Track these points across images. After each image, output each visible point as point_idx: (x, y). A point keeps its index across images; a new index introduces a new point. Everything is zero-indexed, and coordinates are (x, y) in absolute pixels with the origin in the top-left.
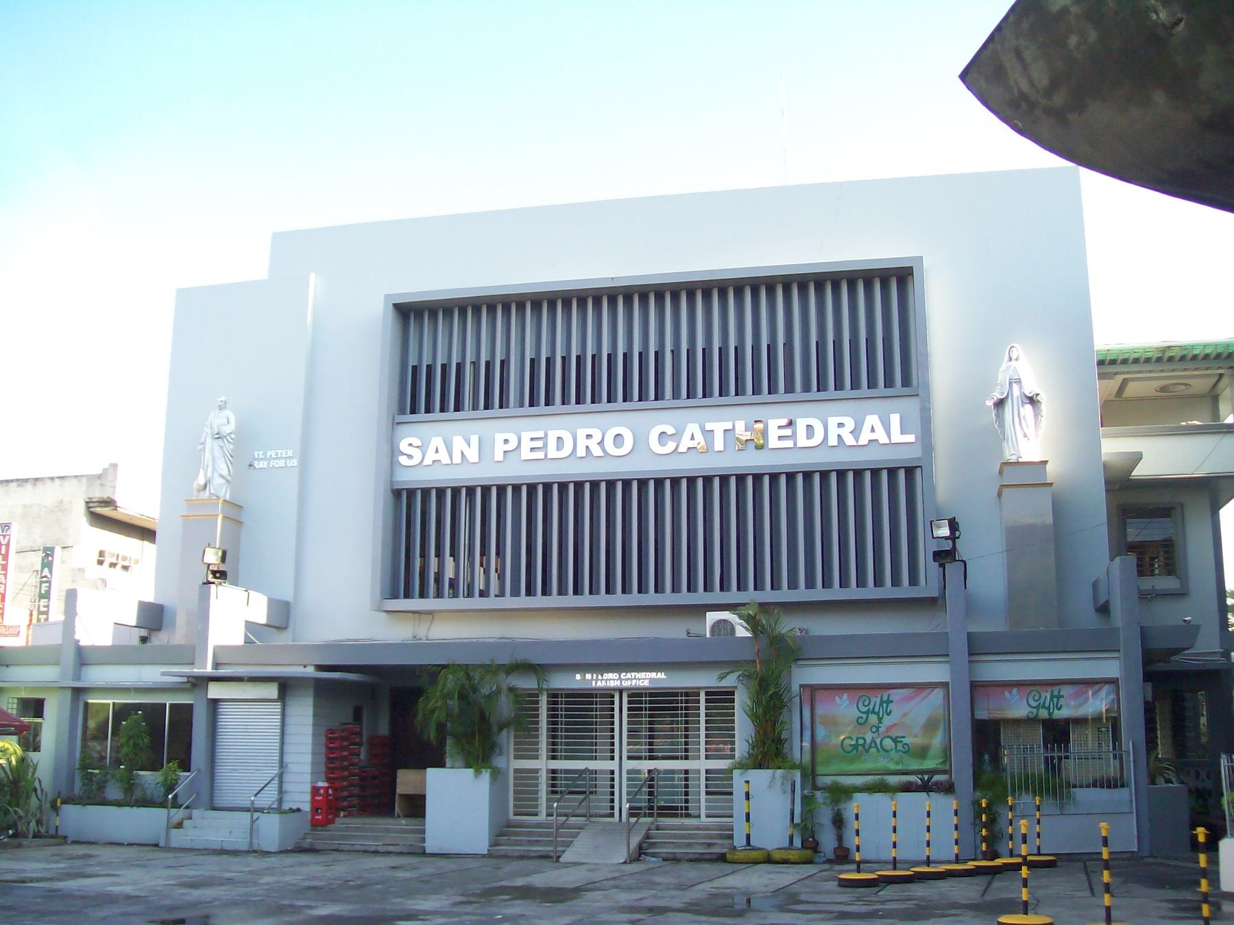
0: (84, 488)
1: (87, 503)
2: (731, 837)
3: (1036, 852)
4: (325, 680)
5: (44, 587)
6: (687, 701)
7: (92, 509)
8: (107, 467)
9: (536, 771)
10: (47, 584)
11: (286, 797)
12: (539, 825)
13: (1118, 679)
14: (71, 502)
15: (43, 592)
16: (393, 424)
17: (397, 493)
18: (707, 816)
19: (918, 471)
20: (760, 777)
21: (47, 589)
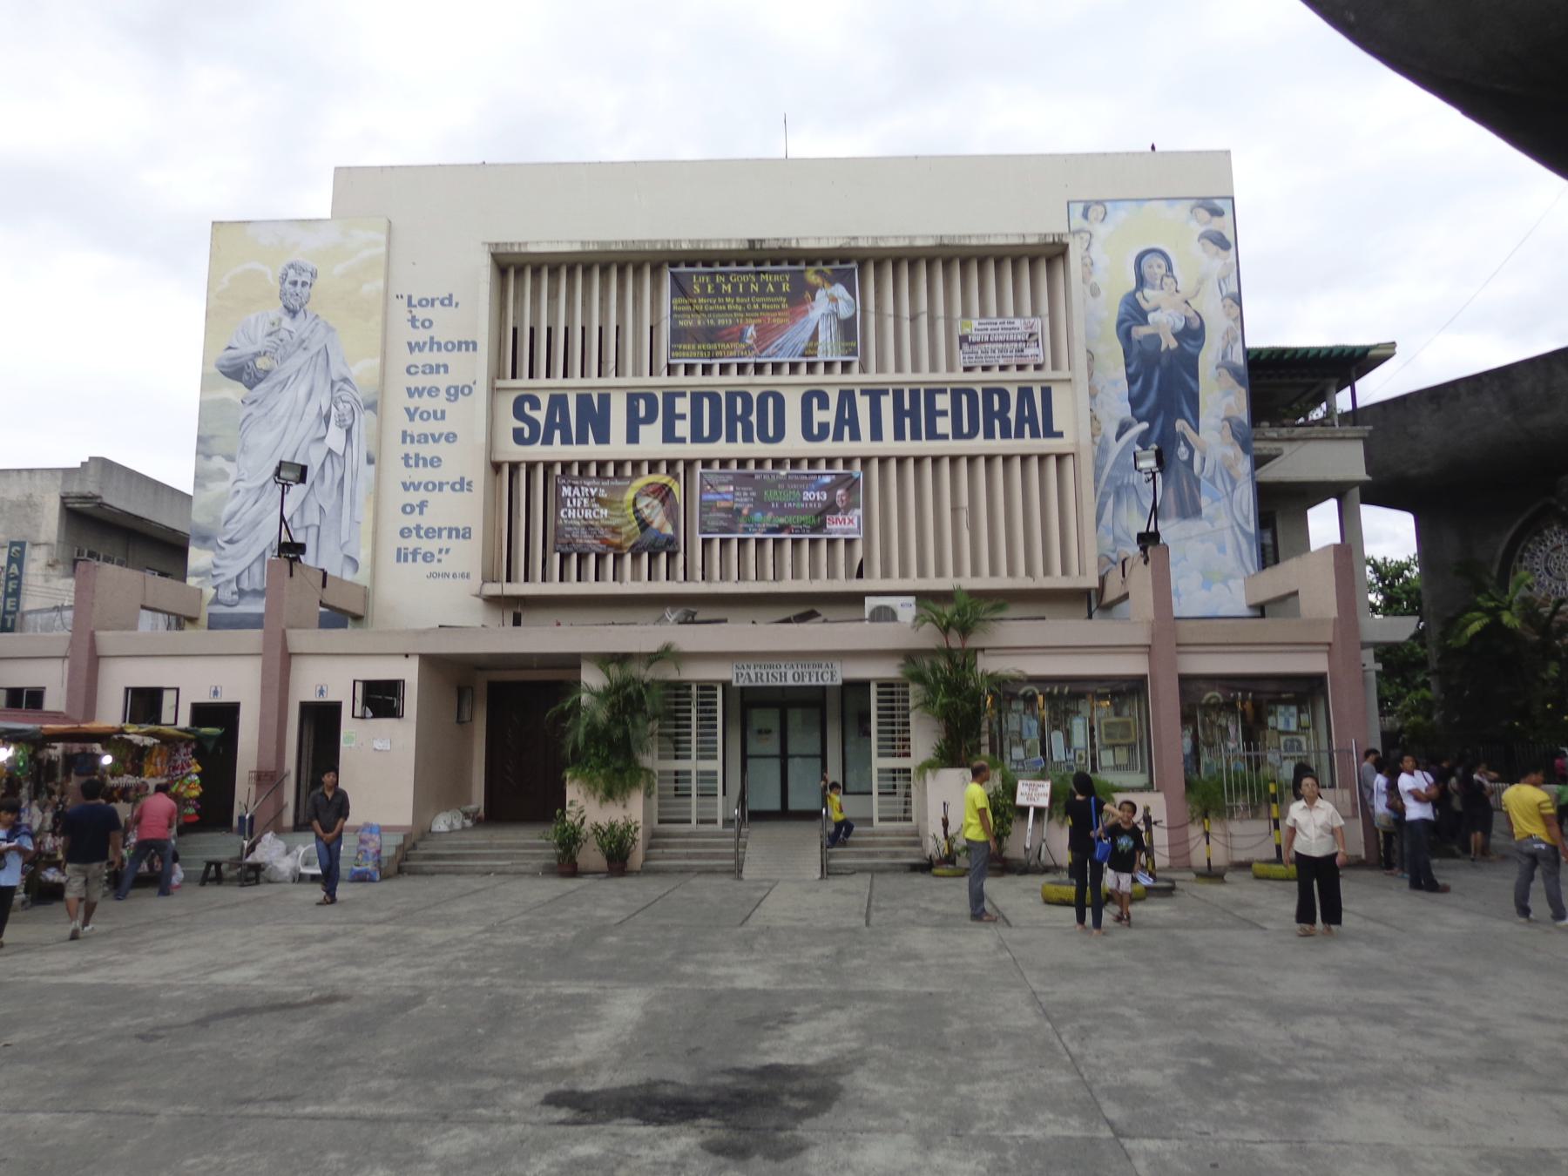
0: (59, 483)
1: (62, 498)
2: (918, 844)
3: (775, 805)
4: (22, 695)
5: (12, 585)
6: (893, 701)
7: (70, 505)
8: (87, 460)
9: (689, 773)
10: (16, 582)
11: (868, 883)
12: (690, 835)
13: (1326, 674)
14: (42, 497)
15: (10, 590)
16: (493, 389)
17: (496, 467)
18: (881, 819)
19: (1069, 462)
20: (953, 778)
21: (15, 587)
